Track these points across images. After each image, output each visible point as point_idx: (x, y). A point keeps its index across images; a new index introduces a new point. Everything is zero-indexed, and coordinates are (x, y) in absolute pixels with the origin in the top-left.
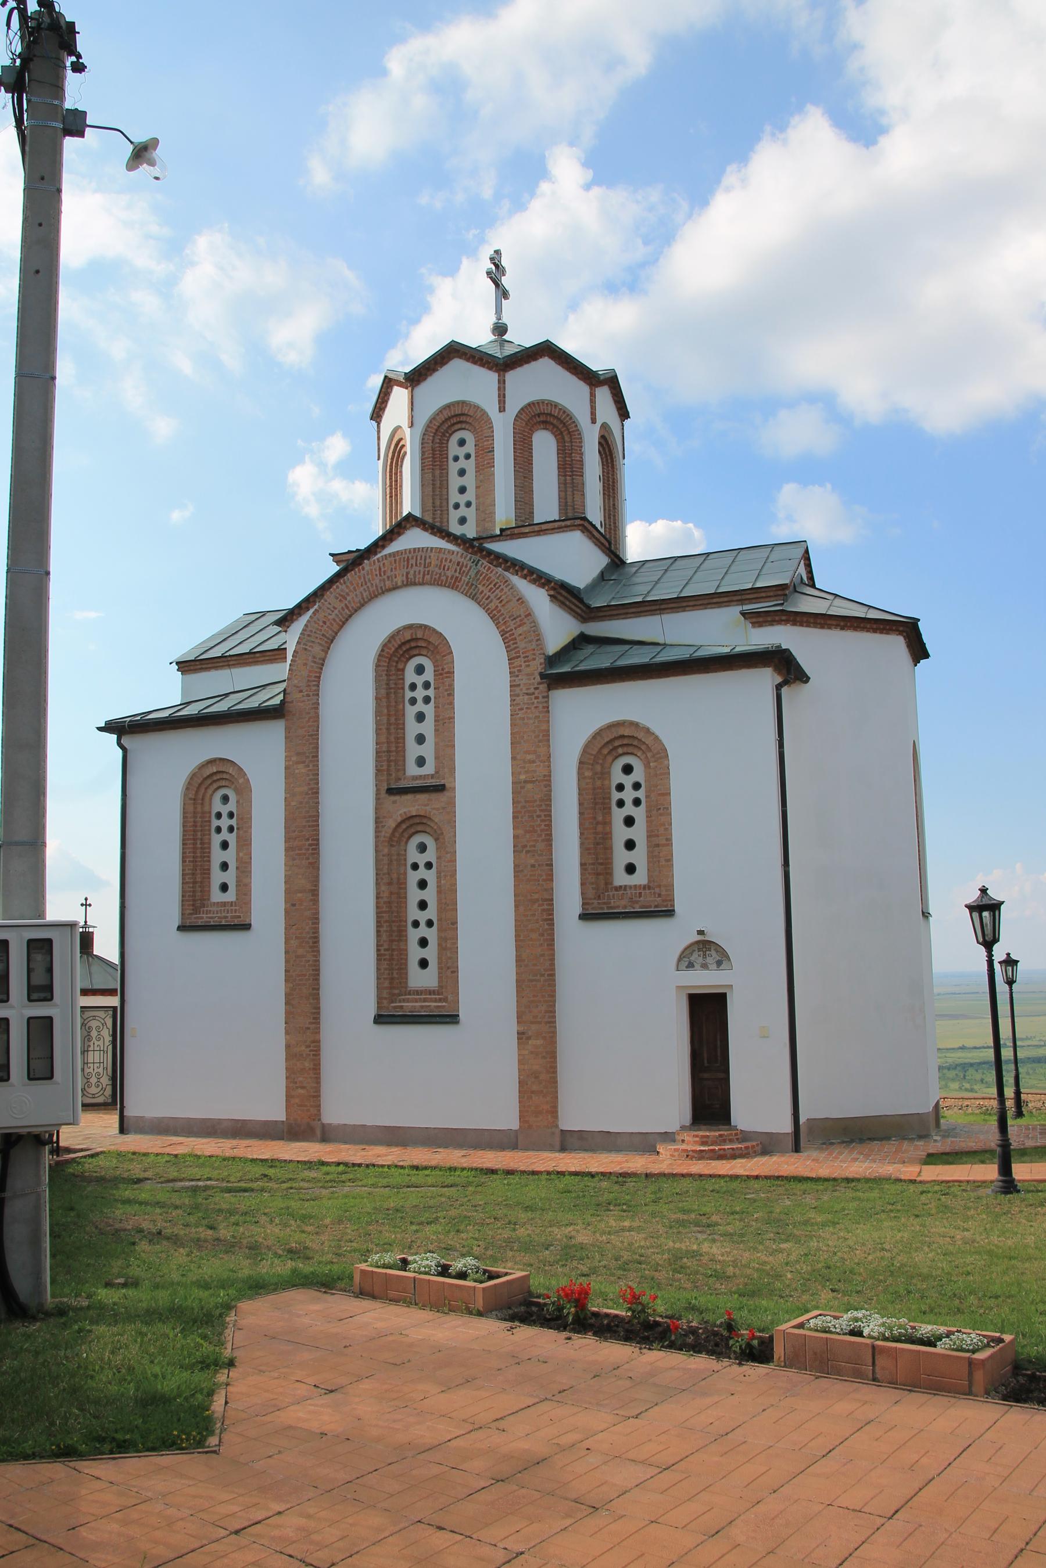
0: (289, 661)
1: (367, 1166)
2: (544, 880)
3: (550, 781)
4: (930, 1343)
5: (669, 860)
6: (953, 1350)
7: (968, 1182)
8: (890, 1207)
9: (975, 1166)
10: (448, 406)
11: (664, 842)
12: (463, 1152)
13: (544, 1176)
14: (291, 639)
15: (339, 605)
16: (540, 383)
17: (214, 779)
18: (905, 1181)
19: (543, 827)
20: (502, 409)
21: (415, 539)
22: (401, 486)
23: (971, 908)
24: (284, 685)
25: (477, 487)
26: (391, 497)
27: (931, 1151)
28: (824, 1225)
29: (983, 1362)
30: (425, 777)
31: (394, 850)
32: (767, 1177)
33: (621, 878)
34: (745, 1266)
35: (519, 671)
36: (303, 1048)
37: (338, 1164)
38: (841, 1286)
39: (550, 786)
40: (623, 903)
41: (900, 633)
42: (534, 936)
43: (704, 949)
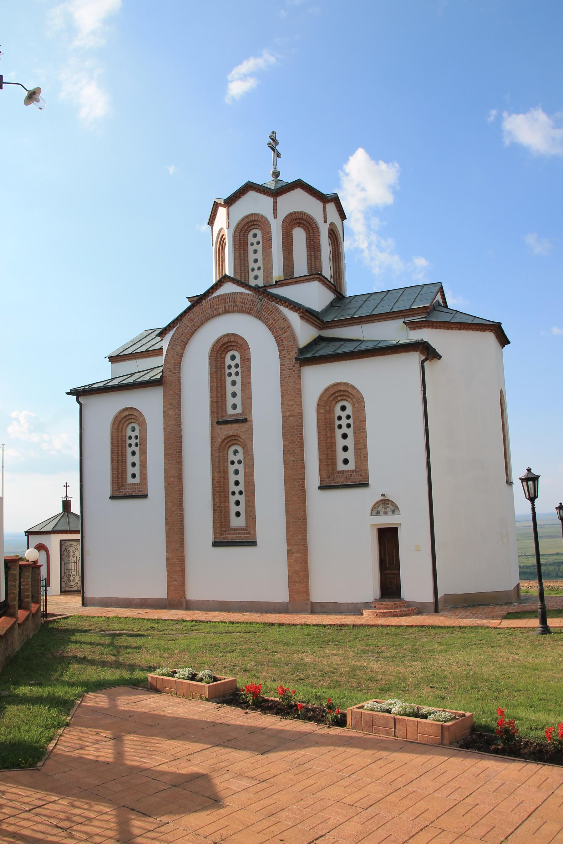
0: (164, 355)
1: (207, 622)
2: (299, 469)
3: (302, 415)
4: (425, 717)
5: (366, 457)
6: (435, 720)
7: (525, 628)
8: (479, 642)
9: (531, 620)
10: (247, 217)
11: (363, 447)
12: (259, 614)
13: (299, 627)
14: (165, 344)
15: (190, 325)
16: (297, 202)
17: (128, 418)
18: (491, 628)
19: (298, 440)
20: (275, 217)
21: (229, 288)
22: (224, 260)
23: (522, 480)
24: (162, 368)
25: (263, 259)
26: (219, 266)
27: (510, 611)
28: (441, 652)
29: (449, 727)
30: (237, 415)
31: (221, 454)
32: (417, 626)
33: (341, 467)
34: (388, 674)
35: (285, 357)
36: (176, 560)
37: (192, 621)
38: (436, 685)
39: (302, 418)
40: (342, 480)
41: (492, 331)
42: (295, 498)
43: (385, 504)
